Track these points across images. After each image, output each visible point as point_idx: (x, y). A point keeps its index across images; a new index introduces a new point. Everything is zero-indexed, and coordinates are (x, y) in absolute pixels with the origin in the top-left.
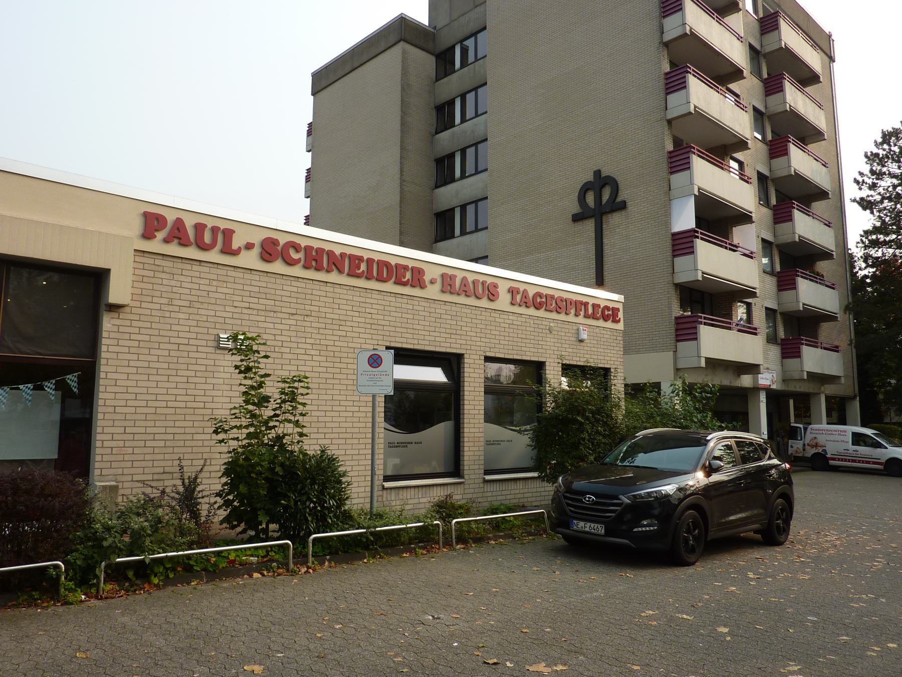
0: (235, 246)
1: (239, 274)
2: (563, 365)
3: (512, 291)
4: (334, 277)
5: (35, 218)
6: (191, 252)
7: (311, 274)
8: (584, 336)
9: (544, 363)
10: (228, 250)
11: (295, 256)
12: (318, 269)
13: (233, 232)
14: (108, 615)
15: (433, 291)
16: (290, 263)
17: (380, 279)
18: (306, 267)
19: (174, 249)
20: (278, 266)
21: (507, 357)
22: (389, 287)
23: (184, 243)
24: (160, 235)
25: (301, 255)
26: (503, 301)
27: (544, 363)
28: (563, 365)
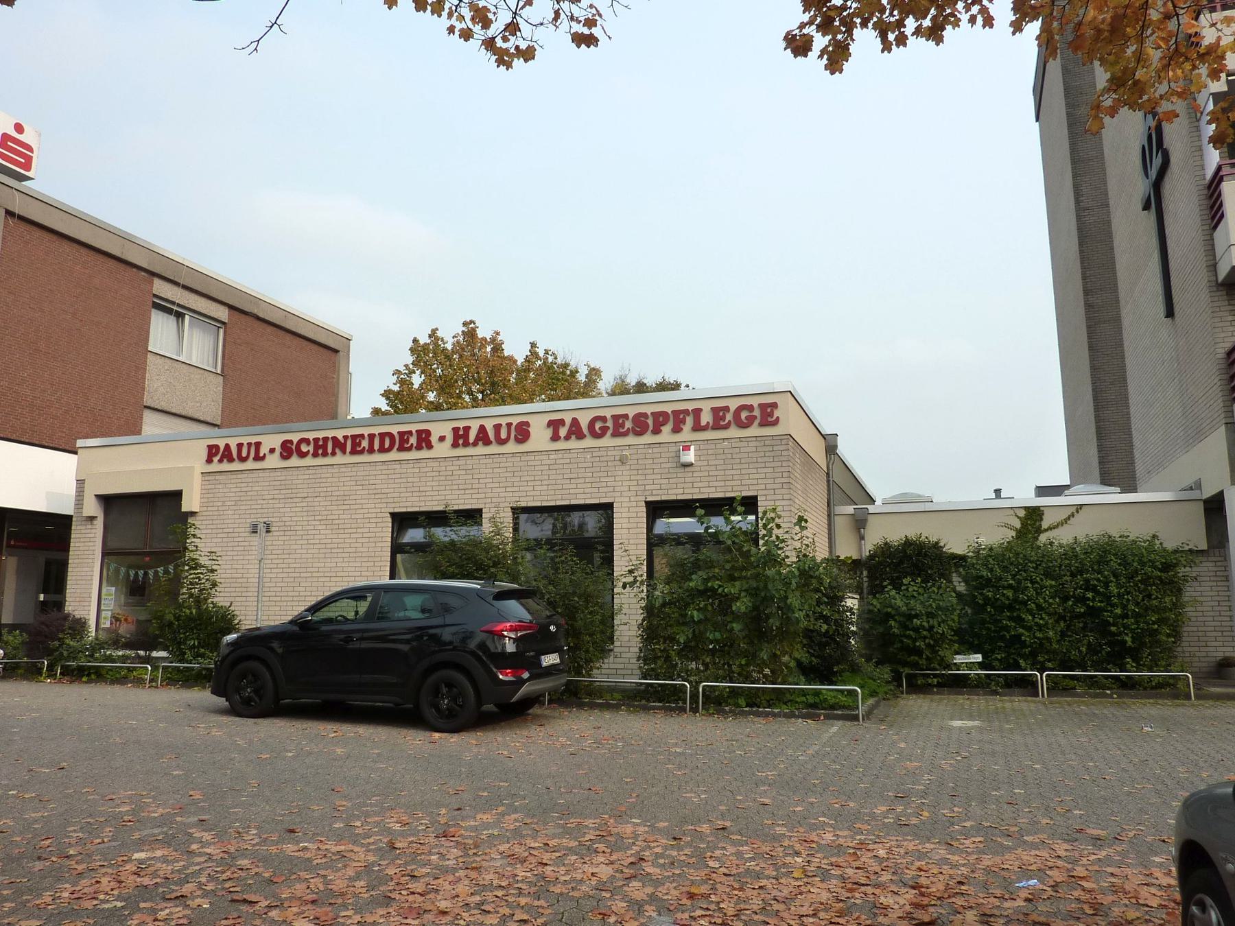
0: (703, 423)
1: (267, 474)
2: (647, 503)
3: (555, 425)
4: (339, 458)
5: (156, 466)
6: (236, 466)
7: (320, 461)
8: (690, 456)
9: (756, 497)
10: (258, 458)
11: (304, 448)
12: (325, 454)
13: (527, 424)
14: (1065, 599)
15: (442, 449)
16: (303, 455)
17: (382, 450)
18: (315, 455)
19: (226, 466)
20: (295, 461)
21: (588, 502)
22: (394, 455)
23: (231, 460)
24: (216, 459)
25: (311, 448)
26: (540, 435)
27: (756, 497)
28: (647, 503)
